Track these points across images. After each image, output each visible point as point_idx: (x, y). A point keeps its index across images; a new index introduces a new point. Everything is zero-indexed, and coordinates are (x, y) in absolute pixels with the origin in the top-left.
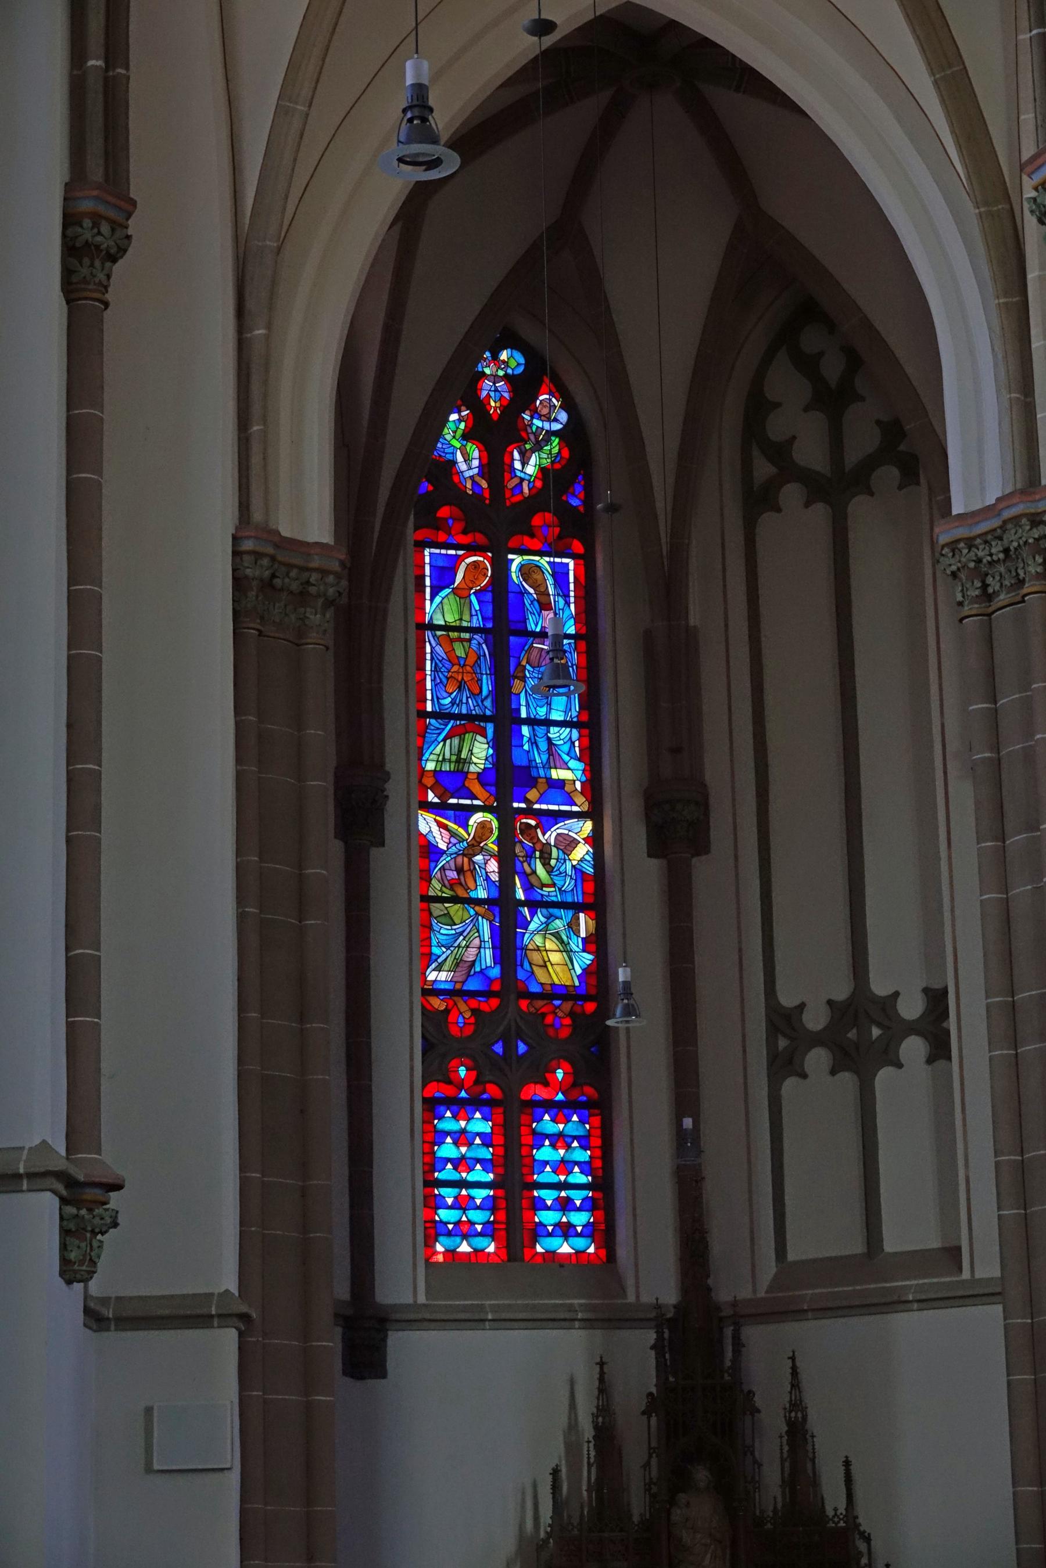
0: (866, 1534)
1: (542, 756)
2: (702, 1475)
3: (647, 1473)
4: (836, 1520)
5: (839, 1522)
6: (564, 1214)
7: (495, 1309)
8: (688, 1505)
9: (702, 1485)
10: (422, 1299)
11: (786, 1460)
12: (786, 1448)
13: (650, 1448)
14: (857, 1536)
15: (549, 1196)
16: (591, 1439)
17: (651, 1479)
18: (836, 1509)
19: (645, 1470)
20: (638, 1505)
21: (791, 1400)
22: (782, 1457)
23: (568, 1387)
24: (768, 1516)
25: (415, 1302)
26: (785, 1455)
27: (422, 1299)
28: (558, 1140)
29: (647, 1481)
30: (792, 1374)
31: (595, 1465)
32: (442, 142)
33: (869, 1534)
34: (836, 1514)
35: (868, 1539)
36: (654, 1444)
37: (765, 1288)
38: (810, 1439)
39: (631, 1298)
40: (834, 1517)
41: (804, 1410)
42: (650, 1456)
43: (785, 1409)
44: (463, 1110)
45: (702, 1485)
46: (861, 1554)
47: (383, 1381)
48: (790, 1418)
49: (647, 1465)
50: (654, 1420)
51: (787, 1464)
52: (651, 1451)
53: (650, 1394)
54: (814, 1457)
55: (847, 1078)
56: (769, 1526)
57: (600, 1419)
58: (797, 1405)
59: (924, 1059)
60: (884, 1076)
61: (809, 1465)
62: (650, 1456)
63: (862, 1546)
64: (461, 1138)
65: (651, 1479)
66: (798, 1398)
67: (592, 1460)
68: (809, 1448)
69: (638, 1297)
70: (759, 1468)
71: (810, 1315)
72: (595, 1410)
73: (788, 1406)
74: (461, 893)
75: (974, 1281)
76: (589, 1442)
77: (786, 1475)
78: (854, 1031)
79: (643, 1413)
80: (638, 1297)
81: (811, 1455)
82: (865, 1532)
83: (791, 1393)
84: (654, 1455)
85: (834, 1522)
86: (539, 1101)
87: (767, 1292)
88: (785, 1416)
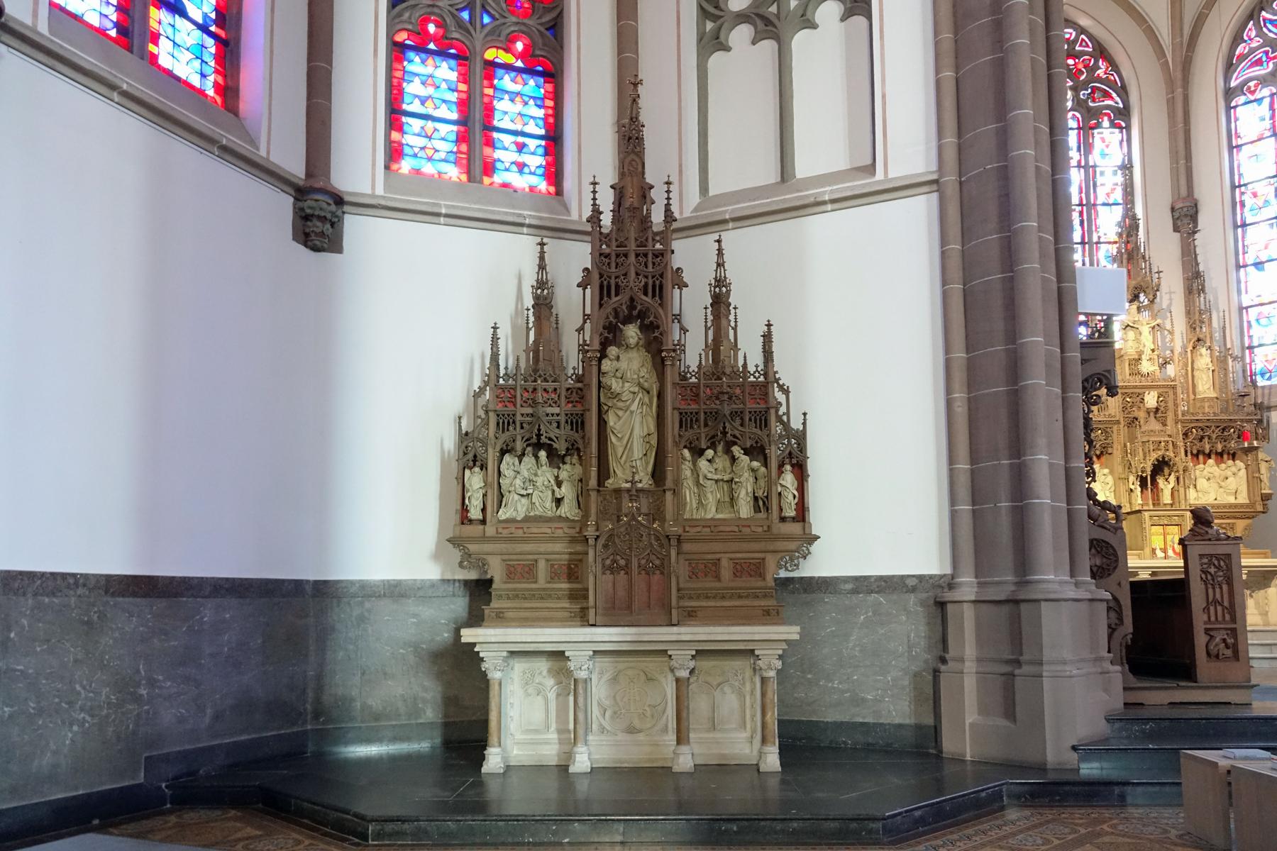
0: (785, 387)
1: (598, 617)
2: (632, 332)
3: (581, 336)
4: (757, 375)
5: (759, 377)
6: (507, 73)
7: (447, 206)
8: (618, 358)
9: (633, 341)
10: (380, 190)
11: (710, 328)
12: (710, 318)
13: (584, 315)
14: (776, 389)
15: (507, 140)
16: (530, 307)
17: (584, 341)
18: (757, 366)
19: (579, 334)
20: (573, 360)
21: (716, 277)
22: (706, 326)
23: (515, 282)
24: (693, 371)
25: (374, 193)
26: (709, 324)
27: (380, 190)
28: (513, 96)
29: (581, 342)
30: (718, 255)
31: (533, 329)
32: (586, 549)
33: (788, 387)
34: (757, 370)
35: (786, 392)
36: (588, 311)
37: (691, 209)
38: (733, 311)
40: (755, 372)
41: (728, 286)
42: (585, 322)
43: (710, 285)
44: (430, 58)
45: (633, 341)
46: (780, 404)
47: (338, 255)
48: (715, 292)
49: (581, 330)
50: (588, 291)
51: (711, 333)
52: (586, 317)
53: (586, 269)
54: (736, 326)
55: (768, 46)
56: (694, 380)
57: (539, 291)
58: (720, 282)
59: (839, 19)
60: (801, 41)
61: (731, 332)
62: (585, 322)
63: (780, 397)
64: (427, 81)
65: (584, 341)
66: (723, 275)
67: (531, 325)
68: (732, 317)
70: (685, 333)
71: (731, 225)
72: (535, 284)
73: (713, 282)
75: (887, 180)
76: (528, 310)
77: (710, 341)
78: (775, 5)
79: (579, 286)
81: (733, 324)
82: (784, 385)
83: (716, 271)
84: (588, 321)
85: (755, 377)
86: (501, 64)
87: (692, 212)
88: (710, 291)
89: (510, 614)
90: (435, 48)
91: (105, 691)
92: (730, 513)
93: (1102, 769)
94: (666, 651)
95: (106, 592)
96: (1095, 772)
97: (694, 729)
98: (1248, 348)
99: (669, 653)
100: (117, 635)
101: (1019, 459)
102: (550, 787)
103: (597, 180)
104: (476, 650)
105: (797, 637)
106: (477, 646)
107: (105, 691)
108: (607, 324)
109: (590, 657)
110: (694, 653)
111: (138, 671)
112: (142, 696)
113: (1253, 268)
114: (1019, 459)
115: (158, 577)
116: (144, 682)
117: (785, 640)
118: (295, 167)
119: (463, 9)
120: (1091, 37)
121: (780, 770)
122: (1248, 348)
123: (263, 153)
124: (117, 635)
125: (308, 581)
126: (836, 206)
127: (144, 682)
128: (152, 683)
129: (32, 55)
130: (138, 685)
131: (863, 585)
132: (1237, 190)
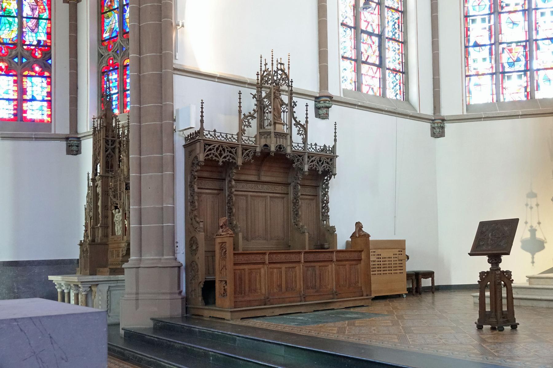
39: (53, 132)
69: (55, 131)
74: (111, 8)
75: (55, 134)
80: (55, 131)
90: (242, 118)
91: (4, 290)
92: (302, 254)
95: (3, 266)
98: (501, 73)
100: (7, 276)
103: (203, 102)
107: (4, 290)
108: (310, 168)
111: (14, 285)
112: (15, 292)
113: (38, 99)
115: (19, 261)
116: (16, 288)
118: (427, 110)
119: (49, 60)
122: (501, 73)
123: (418, 112)
124: (7, 276)
125: (75, 259)
126: (219, 81)
127: (16, 288)
128: (18, 289)
130: (14, 289)
132: (527, 8)
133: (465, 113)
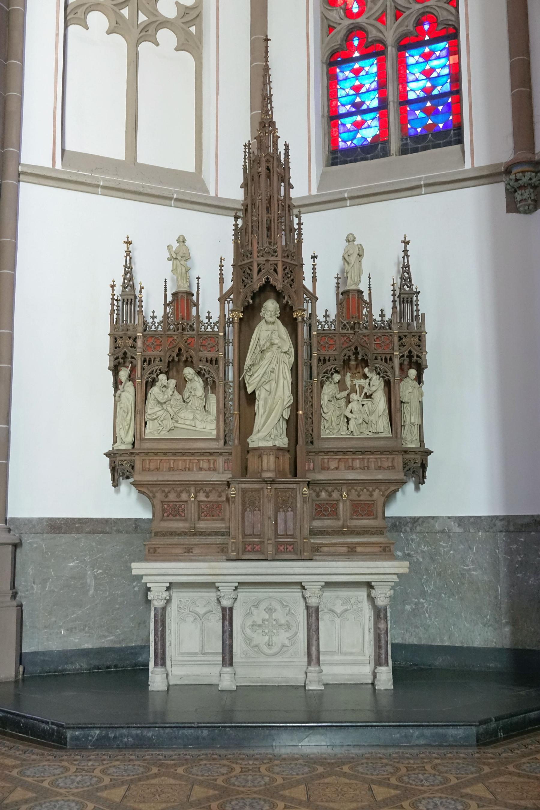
58: (406, 268)
89: (359, 549)
93: (333, 746)
94: (214, 583)
96: (324, 750)
97: (323, 664)
99: (217, 585)
101: (3, 150)
102: (367, 696)
104: (143, 581)
105: (406, 570)
106: (144, 577)
109: (322, 586)
110: (236, 584)
114: (3, 150)
117: (397, 574)
120: (519, 173)
121: (393, 687)
129: (397, 197)
131: (389, 517)
133: (59, 166)
